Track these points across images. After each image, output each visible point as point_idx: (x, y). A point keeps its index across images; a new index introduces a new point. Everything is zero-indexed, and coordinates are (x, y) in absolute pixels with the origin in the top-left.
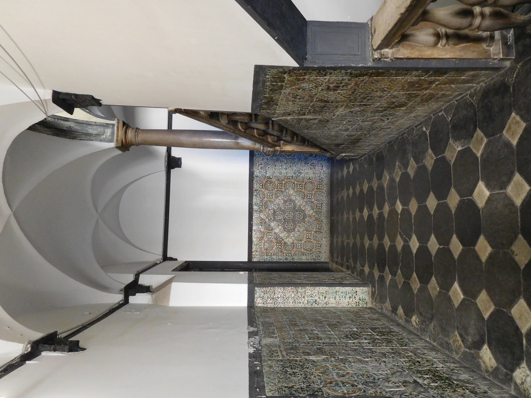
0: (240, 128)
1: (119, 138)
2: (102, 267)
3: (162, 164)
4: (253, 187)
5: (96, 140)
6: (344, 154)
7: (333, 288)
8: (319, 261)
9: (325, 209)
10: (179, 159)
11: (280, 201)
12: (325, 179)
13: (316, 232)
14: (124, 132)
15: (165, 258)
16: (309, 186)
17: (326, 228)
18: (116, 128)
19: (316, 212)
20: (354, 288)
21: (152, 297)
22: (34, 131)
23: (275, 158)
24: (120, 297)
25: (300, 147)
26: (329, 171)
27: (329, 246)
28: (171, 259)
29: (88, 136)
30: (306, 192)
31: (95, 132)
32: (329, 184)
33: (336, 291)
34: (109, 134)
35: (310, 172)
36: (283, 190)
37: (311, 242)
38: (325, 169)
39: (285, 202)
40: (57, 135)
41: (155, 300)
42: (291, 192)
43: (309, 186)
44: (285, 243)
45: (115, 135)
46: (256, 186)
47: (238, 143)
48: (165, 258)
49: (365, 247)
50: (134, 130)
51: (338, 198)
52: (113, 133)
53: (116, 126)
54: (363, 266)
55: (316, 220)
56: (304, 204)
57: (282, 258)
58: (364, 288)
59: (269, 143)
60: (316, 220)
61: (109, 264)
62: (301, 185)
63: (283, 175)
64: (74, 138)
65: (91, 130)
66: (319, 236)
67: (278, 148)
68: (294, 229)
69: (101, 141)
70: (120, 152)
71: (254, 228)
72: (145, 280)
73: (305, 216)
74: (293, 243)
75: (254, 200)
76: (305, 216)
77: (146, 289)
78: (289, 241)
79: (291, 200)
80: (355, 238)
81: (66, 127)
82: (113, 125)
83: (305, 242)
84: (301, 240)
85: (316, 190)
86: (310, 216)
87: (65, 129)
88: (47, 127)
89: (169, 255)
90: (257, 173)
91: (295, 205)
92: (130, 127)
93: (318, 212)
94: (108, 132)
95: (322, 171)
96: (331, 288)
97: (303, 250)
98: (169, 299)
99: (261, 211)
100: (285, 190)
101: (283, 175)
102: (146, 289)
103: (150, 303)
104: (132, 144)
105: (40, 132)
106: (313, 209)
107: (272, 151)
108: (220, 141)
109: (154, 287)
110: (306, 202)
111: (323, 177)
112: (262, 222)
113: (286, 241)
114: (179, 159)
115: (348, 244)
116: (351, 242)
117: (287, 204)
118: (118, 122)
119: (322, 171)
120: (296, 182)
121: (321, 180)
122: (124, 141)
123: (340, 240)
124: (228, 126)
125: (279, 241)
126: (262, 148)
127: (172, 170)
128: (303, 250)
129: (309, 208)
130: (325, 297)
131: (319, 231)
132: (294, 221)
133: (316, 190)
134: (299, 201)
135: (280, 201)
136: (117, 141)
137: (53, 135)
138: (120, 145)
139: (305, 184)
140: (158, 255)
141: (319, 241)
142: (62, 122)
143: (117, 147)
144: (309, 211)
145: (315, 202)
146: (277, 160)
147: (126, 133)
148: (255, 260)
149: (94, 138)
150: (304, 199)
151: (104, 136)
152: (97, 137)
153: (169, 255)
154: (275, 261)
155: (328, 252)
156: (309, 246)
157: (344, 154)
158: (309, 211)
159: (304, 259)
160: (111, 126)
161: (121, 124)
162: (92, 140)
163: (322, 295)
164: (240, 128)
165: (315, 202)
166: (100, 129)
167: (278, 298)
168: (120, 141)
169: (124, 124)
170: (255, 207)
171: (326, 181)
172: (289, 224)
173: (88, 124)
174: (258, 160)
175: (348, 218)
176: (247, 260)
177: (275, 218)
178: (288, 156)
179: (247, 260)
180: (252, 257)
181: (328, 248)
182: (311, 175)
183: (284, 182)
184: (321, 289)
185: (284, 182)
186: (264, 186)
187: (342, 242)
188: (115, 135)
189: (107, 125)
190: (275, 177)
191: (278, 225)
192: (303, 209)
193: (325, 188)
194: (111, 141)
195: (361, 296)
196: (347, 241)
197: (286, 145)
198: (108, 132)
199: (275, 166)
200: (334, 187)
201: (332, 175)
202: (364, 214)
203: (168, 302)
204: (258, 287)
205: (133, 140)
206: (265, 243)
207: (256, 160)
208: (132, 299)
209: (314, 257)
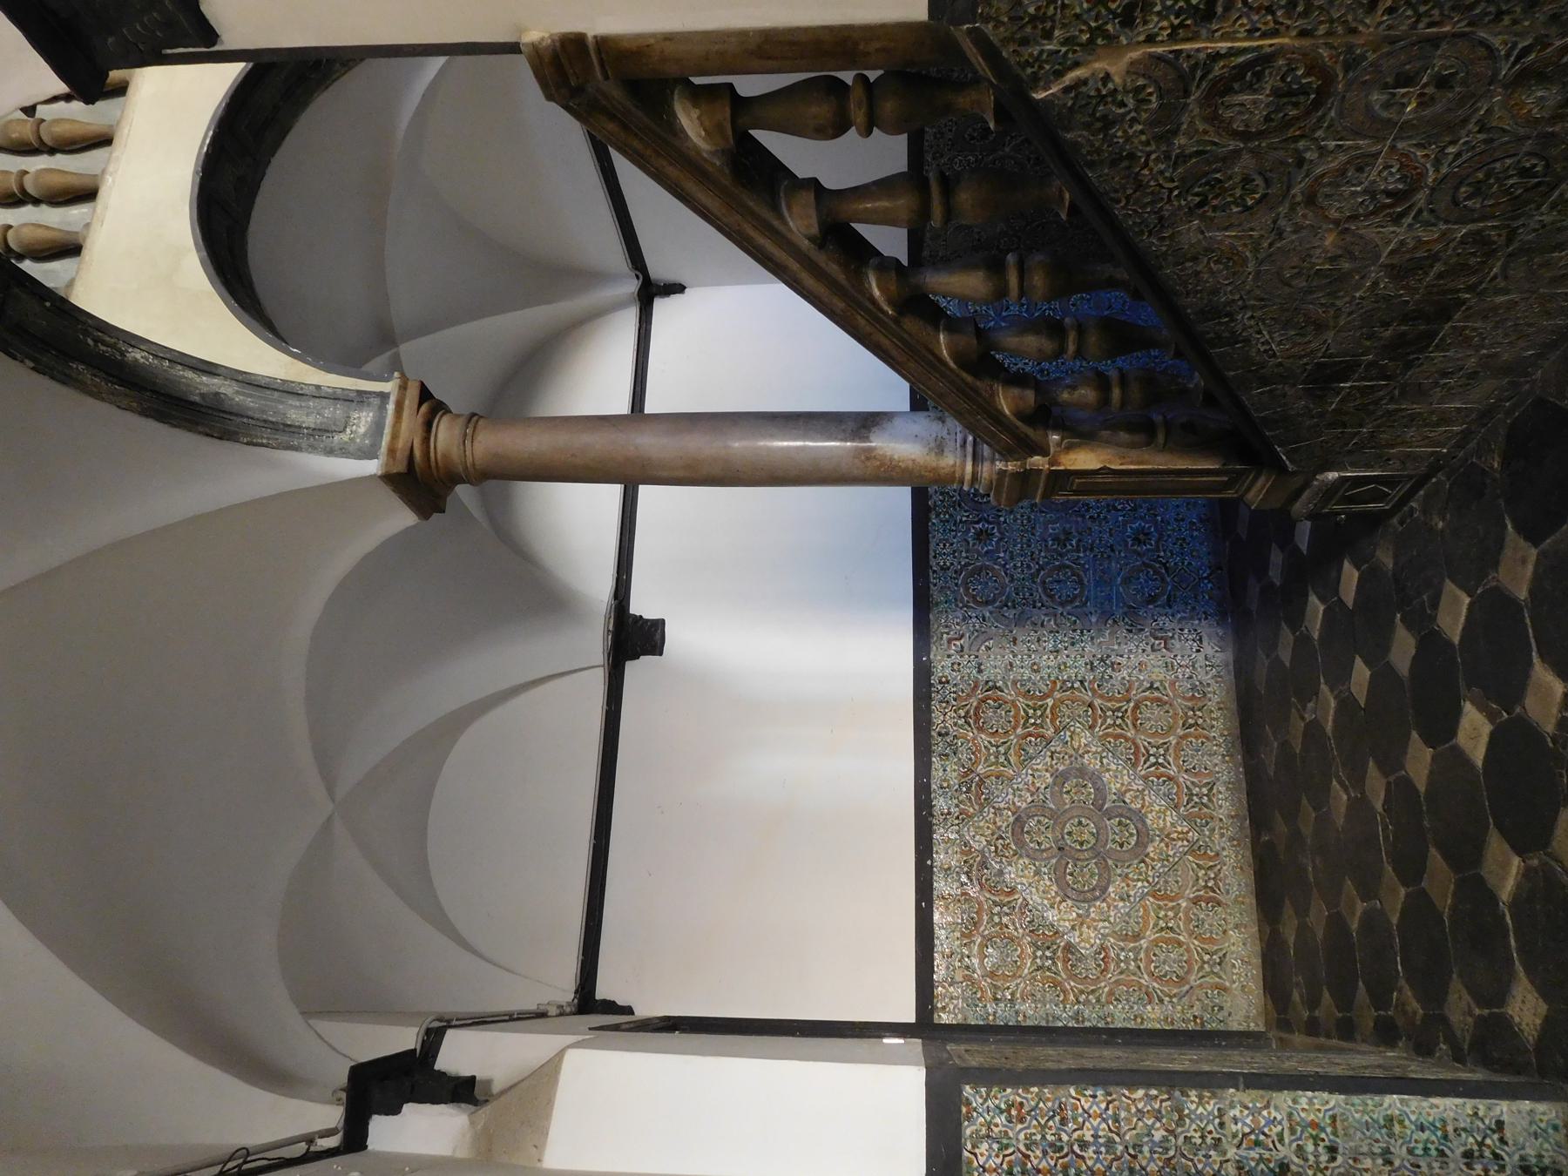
0: (877, 293)
1: (400, 444)
2: (306, 1014)
3: (593, 643)
4: (930, 722)
5: (313, 449)
6: (1332, 475)
7: (1371, 1100)
8: (1221, 1027)
9: (1225, 804)
10: (659, 625)
11: (1041, 772)
12: (1214, 686)
13: (1196, 901)
14: (420, 419)
15: (587, 1001)
16: (1152, 714)
17: (1236, 880)
18: (391, 407)
19: (1188, 818)
20: (1482, 1105)
21: (472, 1123)
22: (64, 383)
23: (1010, 613)
24: (331, 1115)
25: (1134, 454)
26: (1228, 656)
27: (1257, 961)
28: (610, 1007)
29: (285, 435)
30: (1142, 740)
31: (310, 421)
32: (1234, 706)
33: (1390, 1120)
34: (362, 430)
35: (1153, 659)
36: (1050, 732)
37: (1180, 944)
38: (1209, 648)
39: (1060, 778)
40: (161, 417)
41: (486, 1145)
42: (1085, 738)
43: (1152, 714)
44: (1069, 948)
45: (387, 431)
46: (942, 718)
47: (869, 454)
48: (587, 1001)
49: (1493, 898)
50: (461, 421)
51: (1285, 745)
52: (378, 427)
53: (393, 398)
54: (1498, 996)
55: (1191, 851)
56: (1139, 785)
57: (1058, 1012)
58: (1541, 1107)
59: (997, 417)
60: (1191, 851)
61: (331, 996)
62: (1120, 714)
63: (1044, 673)
64: (227, 435)
65: (295, 414)
66: (1211, 919)
67: (1037, 461)
68: (1104, 890)
69: (330, 452)
70: (403, 518)
71: (941, 886)
72: (460, 1054)
73: (1144, 837)
74: (1103, 948)
75: (937, 774)
76: (1144, 837)
77: (463, 1091)
78: (1087, 940)
79: (1082, 772)
80: (1411, 870)
81: (202, 395)
82: (384, 396)
83: (1155, 943)
84: (1137, 937)
85: (1180, 732)
86: (1167, 837)
87: (197, 399)
88: (123, 382)
89: (603, 991)
90: (942, 665)
91: (1101, 791)
92: (448, 411)
93: (1199, 818)
94: (363, 420)
95: (1201, 657)
96: (1356, 1099)
97: (1145, 980)
98: (544, 1133)
99: (964, 817)
100: (1057, 731)
101: (1044, 673)
102: (463, 1091)
103: (462, 1153)
104: (453, 478)
105: (91, 394)
106: (1176, 807)
107: (1015, 475)
108: (797, 448)
109: (496, 1087)
110: (1145, 778)
111: (1207, 679)
112: (975, 866)
113: (1074, 938)
114: (659, 625)
115: (1372, 922)
116: (1395, 899)
117: (1067, 786)
118: (403, 387)
119: (1201, 657)
120: (1097, 702)
121: (1198, 694)
122: (417, 453)
123: (1318, 915)
124: (821, 259)
125: (1046, 939)
126: (969, 468)
127: (630, 667)
128: (1145, 980)
129: (1159, 804)
130: (1332, 1150)
131: (1210, 898)
132: (1099, 854)
133: (1180, 732)
134: (1118, 778)
135: (1041, 772)
136: (392, 451)
137: (145, 413)
138: (400, 467)
139: (1137, 707)
140: (564, 989)
141: (1211, 940)
142: (190, 374)
143: (389, 478)
144: (1160, 815)
145: (1183, 778)
146: (1020, 621)
147: (428, 425)
148: (945, 1018)
149: (304, 443)
150: (1134, 765)
151: (345, 437)
152: (319, 438)
153: (603, 991)
154: (1029, 1023)
155: (1256, 988)
156: (1171, 961)
157: (1332, 475)
158: (1160, 815)
159: (1153, 1017)
160: (376, 401)
161: (413, 393)
162: (297, 449)
163: (1316, 1140)
164: (877, 293)
165: (1183, 778)
166: (332, 412)
167: (1084, 1145)
168: (402, 455)
169: (425, 394)
170: (940, 804)
171: (1218, 694)
172: (1083, 866)
173: (289, 390)
174: (946, 622)
175: (1360, 805)
176: (913, 1020)
177: (1021, 844)
178: (1062, 604)
179: (913, 1020)
180: (934, 1008)
181: (1256, 972)
182: (1158, 674)
183: (1050, 702)
184: (1304, 1102)
185: (1050, 702)
186: (974, 718)
187: (1337, 923)
188: (387, 431)
189: (361, 398)
190: (1015, 683)
191: (1037, 873)
192: (1136, 806)
193: (1219, 724)
194: (368, 454)
195: (1530, 1151)
196: (1360, 907)
197: (1069, 448)
198: (363, 420)
199: (1015, 641)
200: (1255, 714)
201: (1242, 673)
202: (1462, 739)
203: (540, 1147)
204: (976, 1085)
205: (455, 453)
206: (983, 946)
207: (938, 621)
208: (385, 1133)
209: (1196, 1011)
